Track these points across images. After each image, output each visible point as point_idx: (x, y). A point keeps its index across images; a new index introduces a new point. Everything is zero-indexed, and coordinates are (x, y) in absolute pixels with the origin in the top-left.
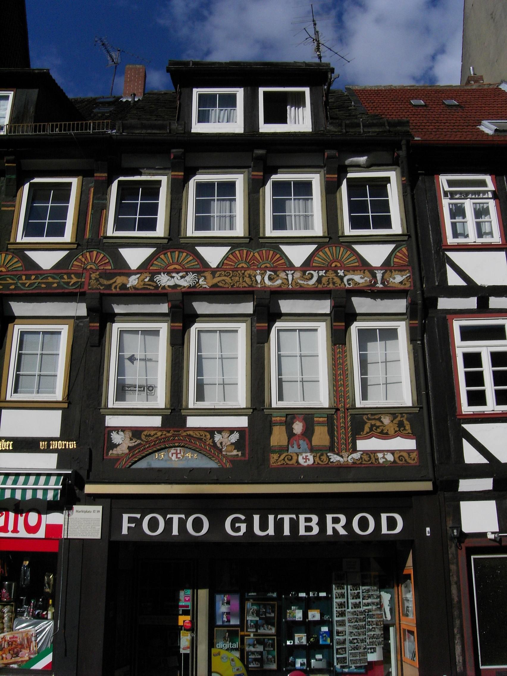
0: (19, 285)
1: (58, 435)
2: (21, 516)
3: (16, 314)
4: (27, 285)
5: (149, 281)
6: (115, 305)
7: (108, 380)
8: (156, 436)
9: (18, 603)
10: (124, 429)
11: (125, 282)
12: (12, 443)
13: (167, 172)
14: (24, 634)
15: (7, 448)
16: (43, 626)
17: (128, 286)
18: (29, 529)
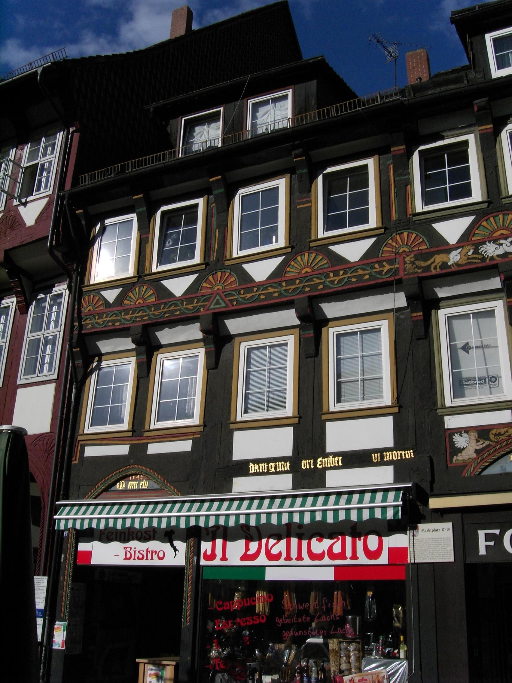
0: (328, 283)
1: (391, 444)
2: (360, 540)
3: (329, 316)
4: (336, 282)
5: (473, 254)
6: (323, 304)
7: (441, 376)
8: (507, 434)
9: (366, 641)
10: (467, 429)
11: (445, 260)
12: (341, 458)
13: (472, 129)
14: (374, 676)
15: (337, 465)
16: (396, 666)
17: (450, 264)
18: (369, 554)
